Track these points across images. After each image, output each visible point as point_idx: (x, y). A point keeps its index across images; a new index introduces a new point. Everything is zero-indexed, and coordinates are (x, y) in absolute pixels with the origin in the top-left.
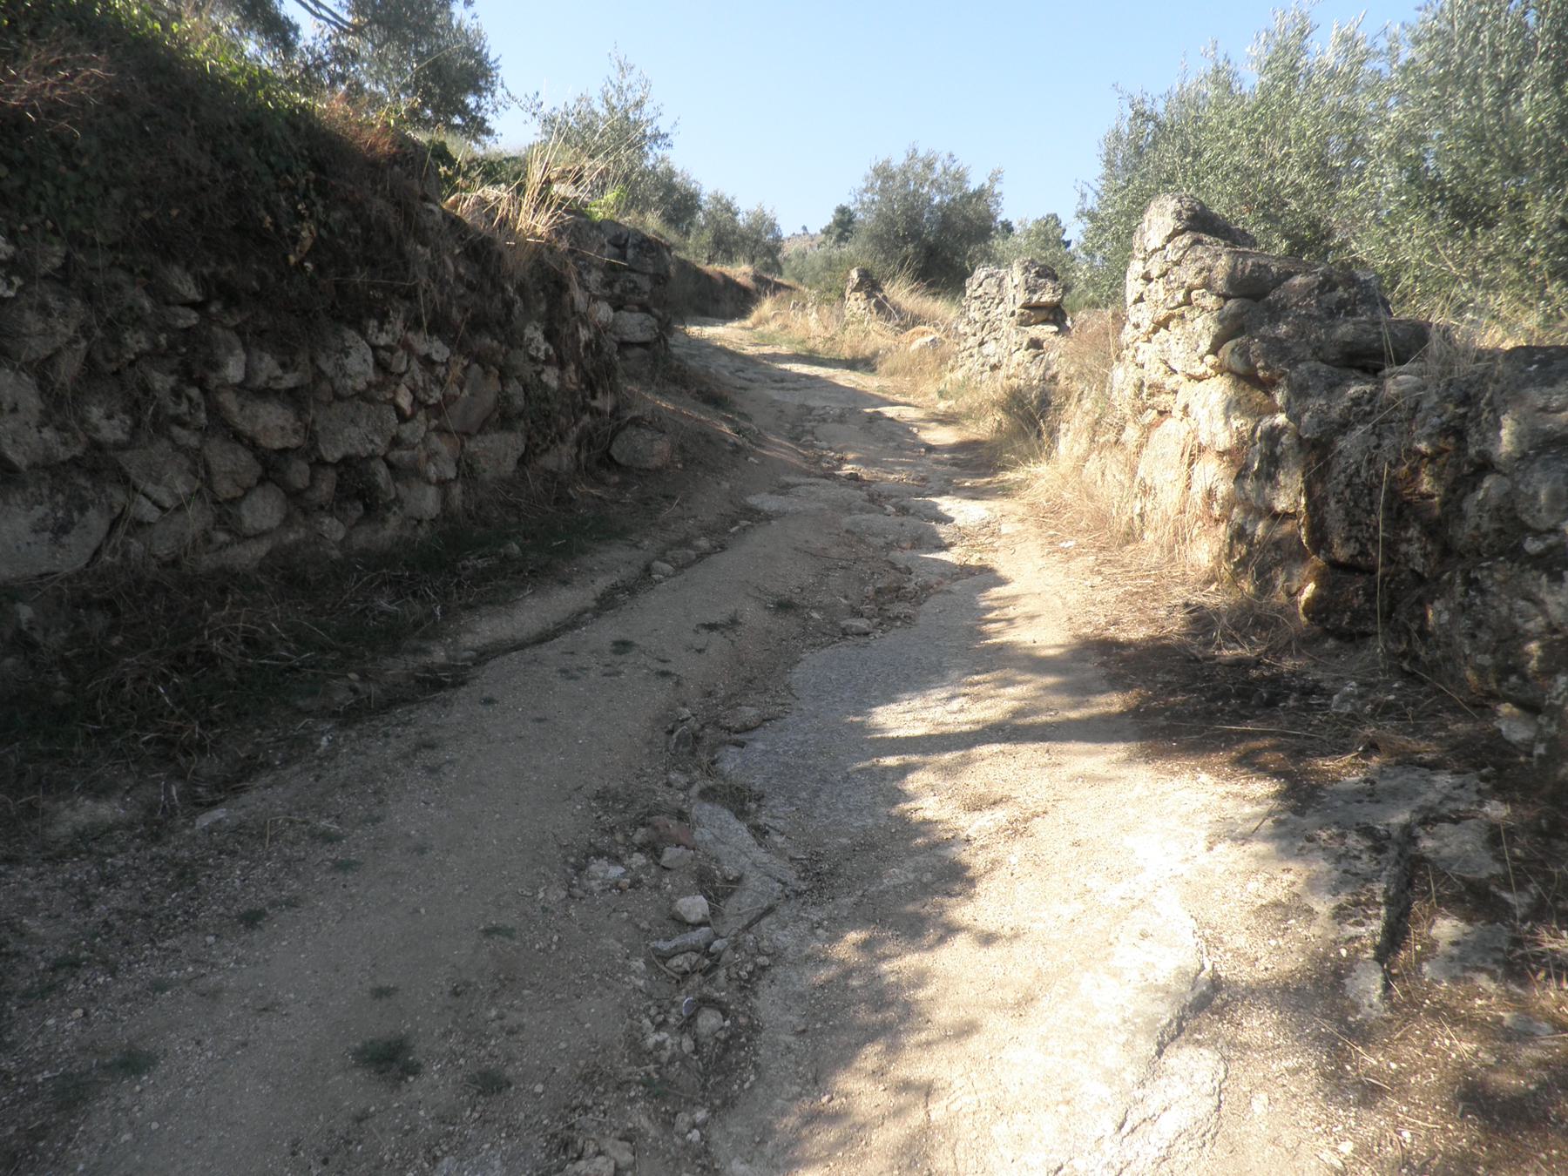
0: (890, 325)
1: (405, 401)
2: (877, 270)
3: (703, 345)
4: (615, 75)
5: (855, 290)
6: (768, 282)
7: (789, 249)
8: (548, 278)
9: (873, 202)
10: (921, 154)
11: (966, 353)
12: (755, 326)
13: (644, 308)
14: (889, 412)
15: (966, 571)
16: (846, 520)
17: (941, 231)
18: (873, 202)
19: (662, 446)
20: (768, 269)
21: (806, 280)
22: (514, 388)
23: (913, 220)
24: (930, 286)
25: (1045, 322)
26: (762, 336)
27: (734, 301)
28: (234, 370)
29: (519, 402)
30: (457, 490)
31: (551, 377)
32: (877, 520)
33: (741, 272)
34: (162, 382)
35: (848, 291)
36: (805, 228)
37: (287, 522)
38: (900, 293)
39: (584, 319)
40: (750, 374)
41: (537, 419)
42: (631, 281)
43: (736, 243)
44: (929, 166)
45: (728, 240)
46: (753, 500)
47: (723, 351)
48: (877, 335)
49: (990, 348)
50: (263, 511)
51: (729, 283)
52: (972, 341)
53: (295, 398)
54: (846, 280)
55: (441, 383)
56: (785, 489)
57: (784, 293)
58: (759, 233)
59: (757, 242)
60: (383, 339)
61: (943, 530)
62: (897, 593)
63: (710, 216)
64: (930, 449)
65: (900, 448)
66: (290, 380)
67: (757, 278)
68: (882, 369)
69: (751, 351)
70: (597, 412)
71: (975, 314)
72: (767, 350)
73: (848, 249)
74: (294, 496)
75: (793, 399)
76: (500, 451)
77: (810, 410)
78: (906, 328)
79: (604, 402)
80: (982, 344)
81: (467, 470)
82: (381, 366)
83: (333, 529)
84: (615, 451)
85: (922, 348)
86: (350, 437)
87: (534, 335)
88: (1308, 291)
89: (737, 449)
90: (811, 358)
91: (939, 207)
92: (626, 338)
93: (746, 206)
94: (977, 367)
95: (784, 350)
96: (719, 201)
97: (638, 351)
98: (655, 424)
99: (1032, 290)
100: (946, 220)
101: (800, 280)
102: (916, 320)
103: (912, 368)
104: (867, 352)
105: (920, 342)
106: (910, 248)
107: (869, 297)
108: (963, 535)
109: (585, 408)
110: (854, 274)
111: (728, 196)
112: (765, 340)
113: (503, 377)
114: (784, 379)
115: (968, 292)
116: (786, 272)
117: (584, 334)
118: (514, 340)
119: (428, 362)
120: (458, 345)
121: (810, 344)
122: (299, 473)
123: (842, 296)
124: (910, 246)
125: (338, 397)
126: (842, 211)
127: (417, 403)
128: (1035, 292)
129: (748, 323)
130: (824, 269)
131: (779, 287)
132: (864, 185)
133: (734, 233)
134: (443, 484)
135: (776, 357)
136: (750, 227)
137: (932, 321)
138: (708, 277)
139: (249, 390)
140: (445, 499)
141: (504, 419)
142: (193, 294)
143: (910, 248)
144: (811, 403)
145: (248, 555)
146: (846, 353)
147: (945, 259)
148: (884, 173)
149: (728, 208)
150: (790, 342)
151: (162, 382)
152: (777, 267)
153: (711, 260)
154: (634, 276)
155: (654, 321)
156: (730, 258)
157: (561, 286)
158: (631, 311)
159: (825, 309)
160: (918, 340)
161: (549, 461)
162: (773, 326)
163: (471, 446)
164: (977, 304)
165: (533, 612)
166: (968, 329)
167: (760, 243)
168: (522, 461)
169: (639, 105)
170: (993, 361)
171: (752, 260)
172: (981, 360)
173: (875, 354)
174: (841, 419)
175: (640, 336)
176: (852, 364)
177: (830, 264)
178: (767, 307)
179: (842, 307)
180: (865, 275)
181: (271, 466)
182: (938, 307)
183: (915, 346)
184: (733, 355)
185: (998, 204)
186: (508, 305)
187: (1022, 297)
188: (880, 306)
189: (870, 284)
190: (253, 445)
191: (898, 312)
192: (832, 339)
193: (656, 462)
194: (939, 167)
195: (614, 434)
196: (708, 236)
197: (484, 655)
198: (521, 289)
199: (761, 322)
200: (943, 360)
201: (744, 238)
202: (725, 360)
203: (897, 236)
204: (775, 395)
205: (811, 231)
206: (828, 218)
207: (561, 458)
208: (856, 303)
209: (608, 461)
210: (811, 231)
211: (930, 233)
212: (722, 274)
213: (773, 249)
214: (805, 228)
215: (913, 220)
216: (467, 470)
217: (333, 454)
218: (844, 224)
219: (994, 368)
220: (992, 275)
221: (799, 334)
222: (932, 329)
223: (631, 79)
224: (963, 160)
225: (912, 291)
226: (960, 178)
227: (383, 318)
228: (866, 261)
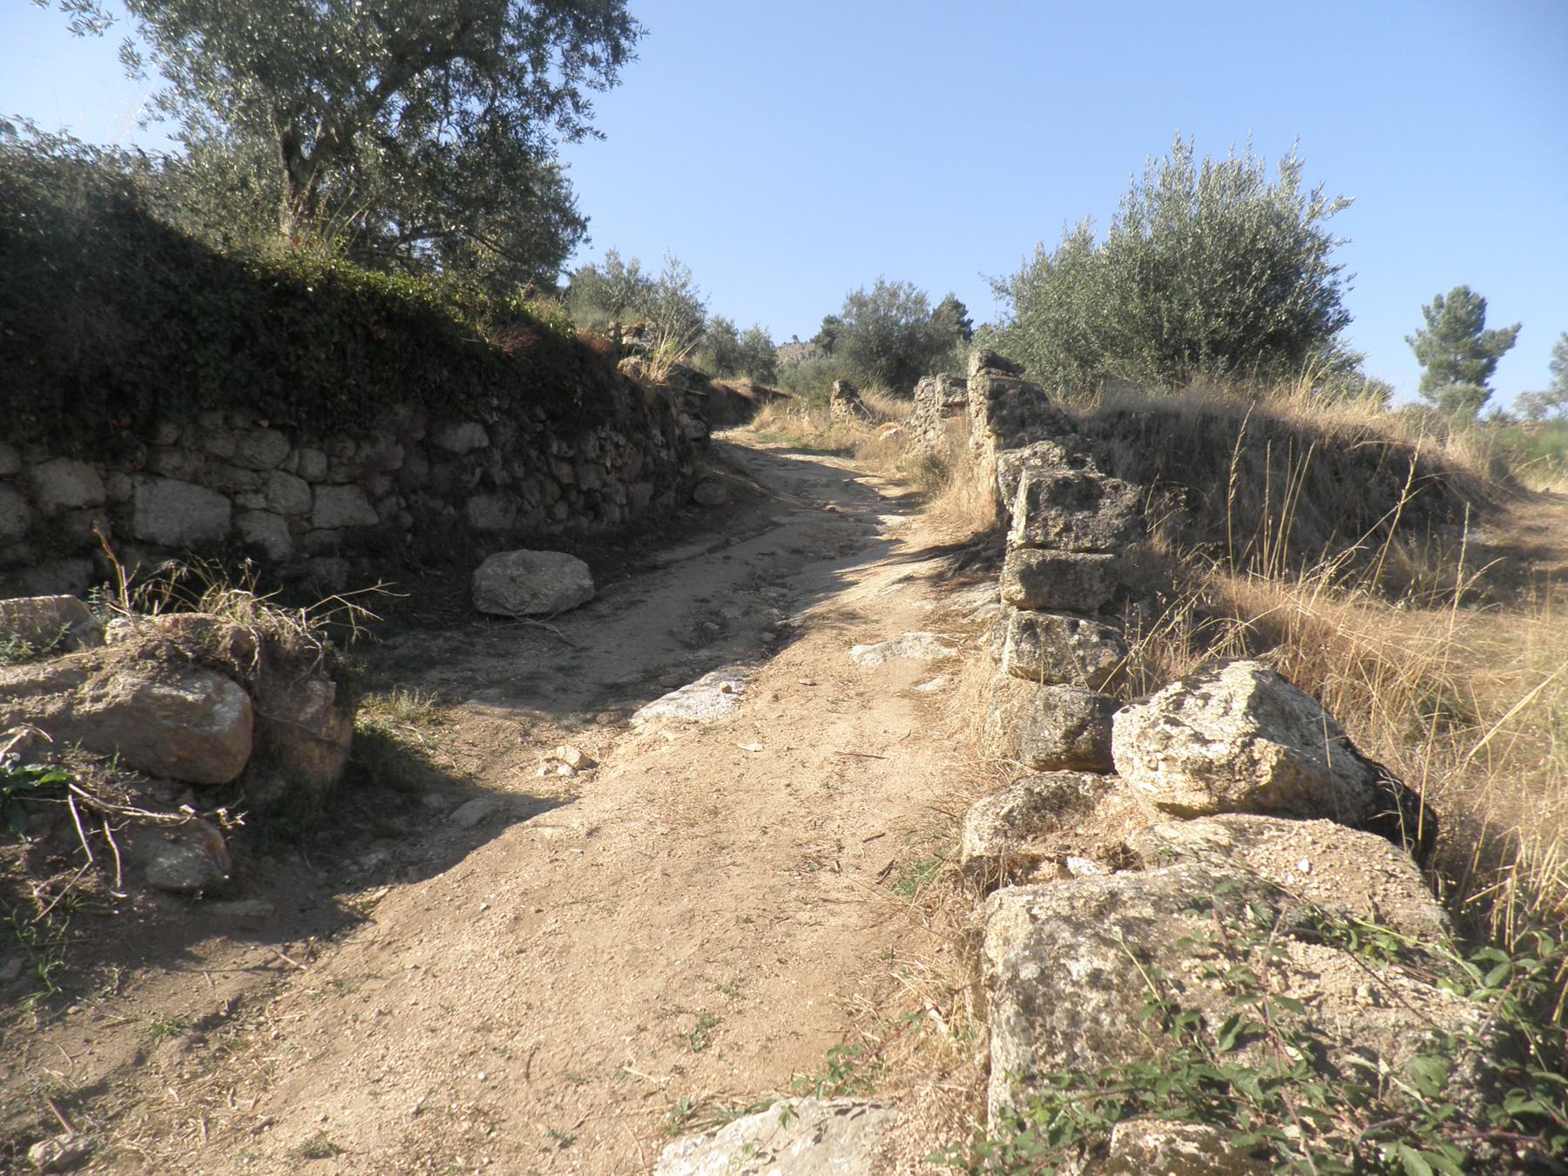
1: (608, 464)
2: (855, 382)
3: (725, 444)
4: (668, 268)
5: (837, 397)
6: (766, 392)
7: (783, 359)
8: (662, 400)
10: (887, 284)
12: (757, 430)
14: (860, 480)
15: (890, 541)
16: (826, 525)
19: (722, 491)
20: (764, 380)
21: (799, 388)
22: (649, 459)
24: (897, 391)
26: (765, 436)
27: (742, 409)
28: (555, 449)
29: (651, 466)
30: (627, 510)
31: (664, 454)
32: (844, 525)
33: (742, 384)
34: (534, 453)
36: (795, 337)
37: (568, 518)
38: (875, 398)
39: (677, 423)
40: (761, 462)
41: (656, 475)
43: (736, 360)
44: (894, 295)
46: (774, 519)
47: (737, 447)
48: (857, 431)
50: (561, 511)
51: (731, 393)
53: (572, 461)
54: (830, 389)
55: (621, 456)
56: (793, 514)
57: (781, 401)
59: (754, 357)
60: (603, 435)
61: (879, 528)
62: (850, 547)
63: (714, 338)
64: (884, 498)
65: (864, 499)
66: (571, 454)
67: (755, 389)
68: (859, 455)
69: (759, 447)
70: (684, 476)
71: (920, 412)
72: (772, 445)
73: (834, 359)
74: (571, 505)
75: (794, 476)
76: (644, 490)
77: (805, 482)
79: (688, 470)
81: (631, 502)
82: (602, 448)
83: (584, 522)
84: (696, 496)
86: (591, 481)
87: (656, 432)
88: (1014, 395)
89: (763, 496)
90: (805, 450)
93: (743, 325)
95: (785, 445)
96: (719, 324)
98: (716, 480)
100: (910, 336)
101: (793, 388)
103: (880, 453)
105: (886, 433)
106: (883, 361)
107: (849, 402)
108: (890, 529)
109: (679, 473)
110: (837, 385)
111: (728, 320)
112: (765, 439)
113: (645, 454)
114: (787, 463)
116: (780, 382)
117: (677, 432)
118: (649, 436)
119: (617, 445)
120: (628, 437)
121: (805, 441)
122: (573, 496)
123: (828, 402)
125: (586, 461)
126: (830, 321)
127: (613, 465)
129: (752, 427)
130: (815, 378)
131: (776, 395)
134: (621, 506)
135: (778, 450)
137: (895, 418)
139: (560, 458)
140: (622, 514)
141: (644, 476)
142: (543, 417)
143: (883, 361)
145: (558, 529)
146: (833, 446)
148: (858, 301)
149: (728, 330)
150: (788, 440)
151: (534, 453)
152: (772, 379)
156: (732, 373)
157: (667, 407)
159: (815, 412)
160: (885, 433)
161: (663, 500)
162: (773, 429)
163: (631, 489)
165: (680, 553)
168: (652, 498)
169: (684, 286)
171: (750, 373)
173: (854, 445)
174: (827, 485)
176: (836, 453)
177: (820, 373)
178: (767, 413)
179: (828, 410)
180: (845, 386)
181: (564, 490)
182: (903, 406)
184: (746, 450)
186: (645, 417)
187: (942, 399)
188: (857, 409)
189: (849, 392)
190: (559, 483)
193: (719, 501)
194: (903, 297)
195: (695, 487)
197: (667, 564)
198: (651, 409)
199: (762, 426)
201: (743, 355)
202: (740, 454)
204: (781, 473)
205: (802, 339)
206: (816, 329)
207: (669, 498)
208: (839, 408)
209: (692, 502)
210: (802, 339)
214: (795, 337)
216: (631, 502)
217: (585, 488)
218: (830, 338)
221: (795, 435)
223: (679, 270)
224: (921, 286)
226: (920, 301)
227: (603, 425)
228: (843, 374)
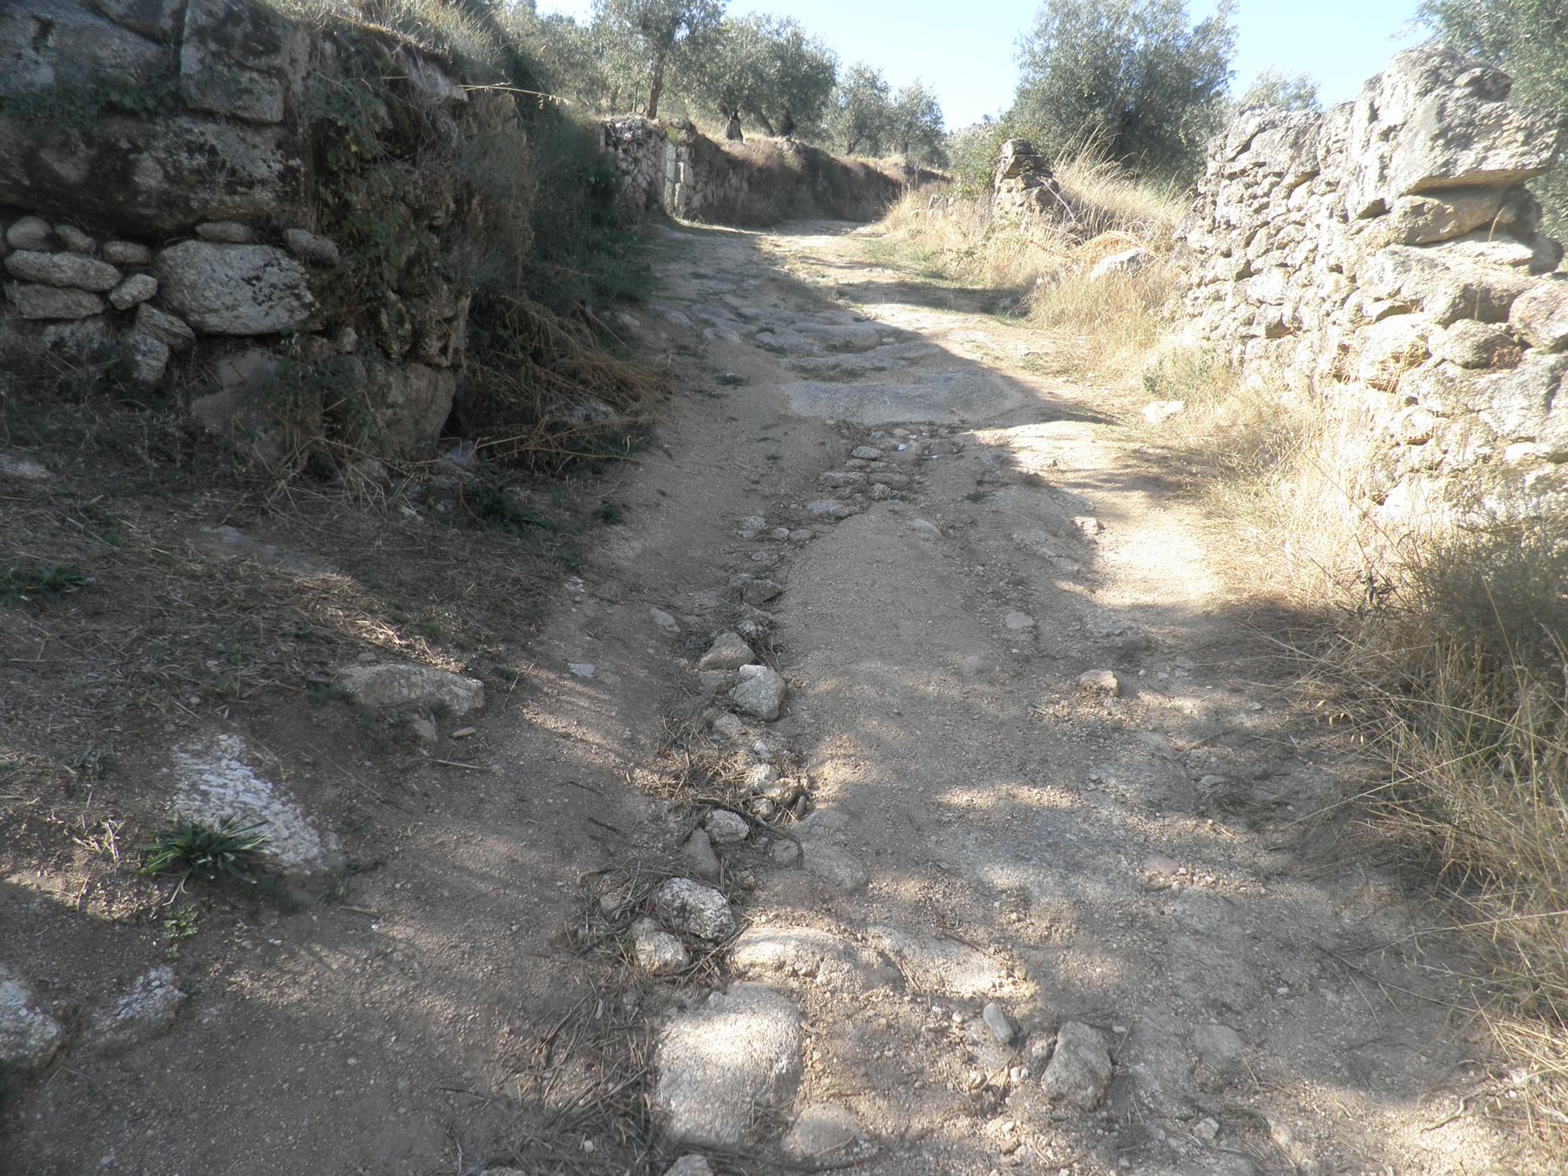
0: (1062, 229)
2: (1046, 142)
5: (1008, 175)
9: (1048, 50)
11: (1205, 291)
13: (268, 232)
17: (1145, 88)
18: (1048, 50)
23: (1103, 71)
24: (1127, 164)
25: (1481, 231)
33: (891, 163)
35: (999, 176)
38: (1081, 179)
42: (194, 149)
43: (881, 128)
45: (872, 124)
49: (1268, 284)
52: (1221, 267)
58: (913, 113)
78: (1086, 234)
80: (1245, 273)
85: (1112, 275)
91: (1144, 54)
92: (214, 322)
94: (1230, 325)
96: (860, 73)
97: (255, 360)
99: (1454, 138)
102: (1107, 220)
104: (1020, 279)
110: (1008, 150)
115: (1212, 167)
123: (990, 185)
124: (1098, 111)
128: (1465, 142)
132: (1036, 27)
133: (880, 114)
136: (902, 107)
138: (846, 170)
144: (872, 416)
146: (985, 280)
147: (1148, 129)
153: (850, 151)
154: (208, 132)
155: (295, 271)
158: (221, 241)
160: (1107, 257)
164: (1237, 188)
166: (1210, 241)
167: (917, 129)
170: (1272, 314)
172: (1243, 312)
173: (1030, 285)
175: (254, 318)
178: (907, 205)
180: (1025, 151)
182: (1137, 197)
183: (1100, 270)
185: (1230, 44)
188: (1045, 200)
191: (1076, 209)
192: (970, 253)
196: (847, 118)
200: (1154, 300)
203: (1080, 98)
208: (1011, 196)
211: (1128, 91)
212: (865, 167)
213: (931, 137)
214: (986, 117)
215: (1103, 71)
219: (1277, 330)
220: (1273, 125)
222: (1131, 235)
225: (1100, 174)
